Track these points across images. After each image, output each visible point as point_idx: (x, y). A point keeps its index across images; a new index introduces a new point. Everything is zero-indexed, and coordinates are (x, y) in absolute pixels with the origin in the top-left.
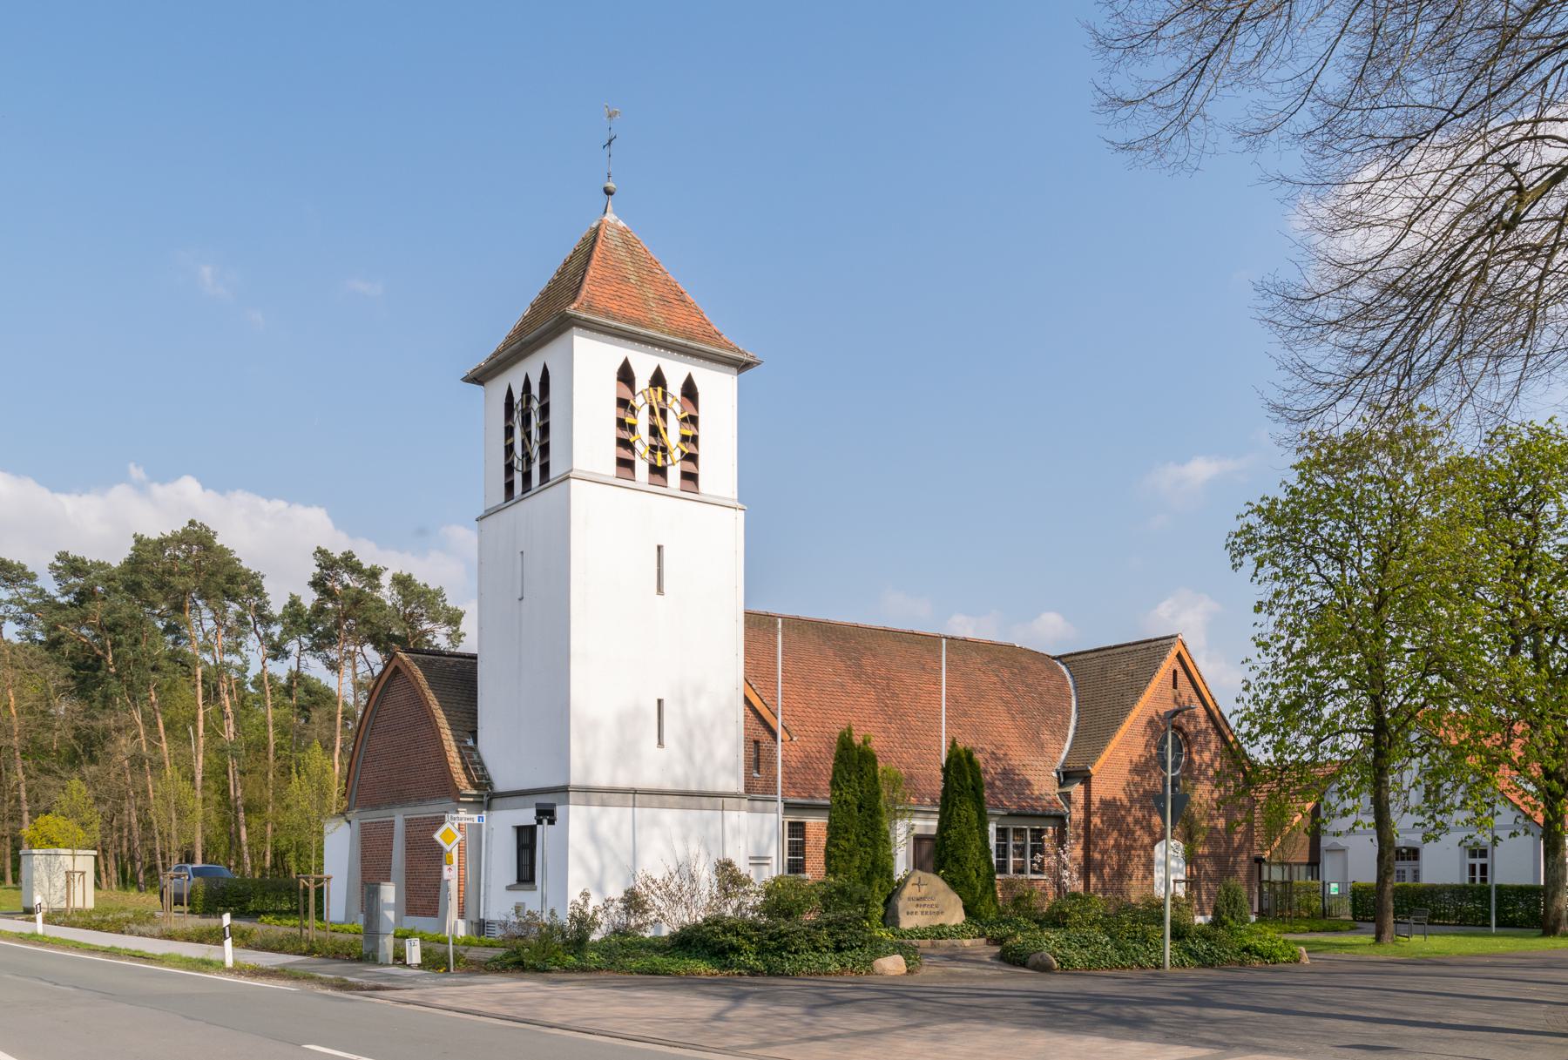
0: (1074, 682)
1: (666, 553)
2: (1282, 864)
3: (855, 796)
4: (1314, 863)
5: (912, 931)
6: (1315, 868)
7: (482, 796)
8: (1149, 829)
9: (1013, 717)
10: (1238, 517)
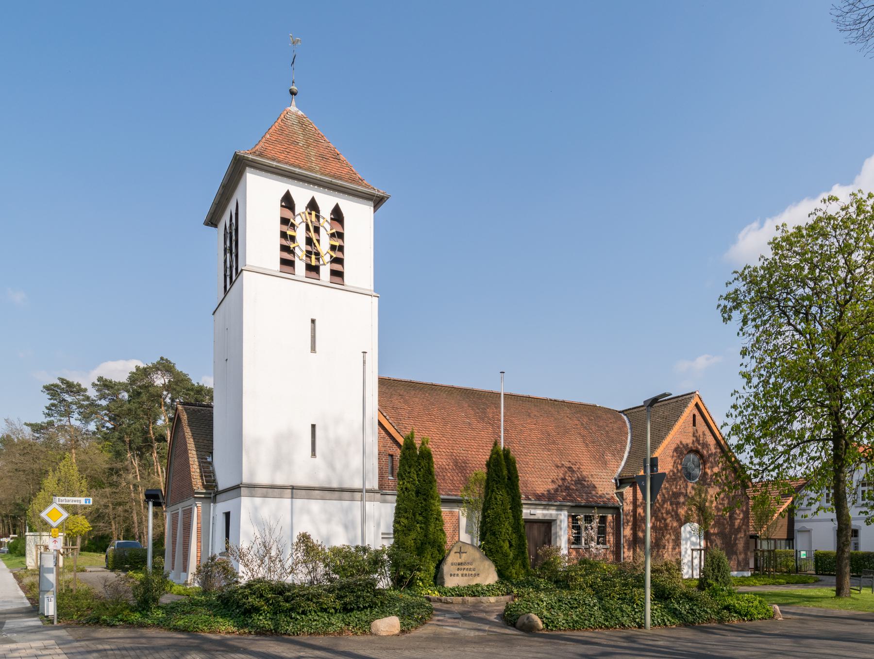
0: (631, 425)
1: (317, 323)
2: (768, 539)
3: (414, 484)
4: (790, 539)
5: (453, 589)
6: (791, 542)
7: (210, 494)
8: (677, 517)
9: (587, 445)
10: (727, 284)
